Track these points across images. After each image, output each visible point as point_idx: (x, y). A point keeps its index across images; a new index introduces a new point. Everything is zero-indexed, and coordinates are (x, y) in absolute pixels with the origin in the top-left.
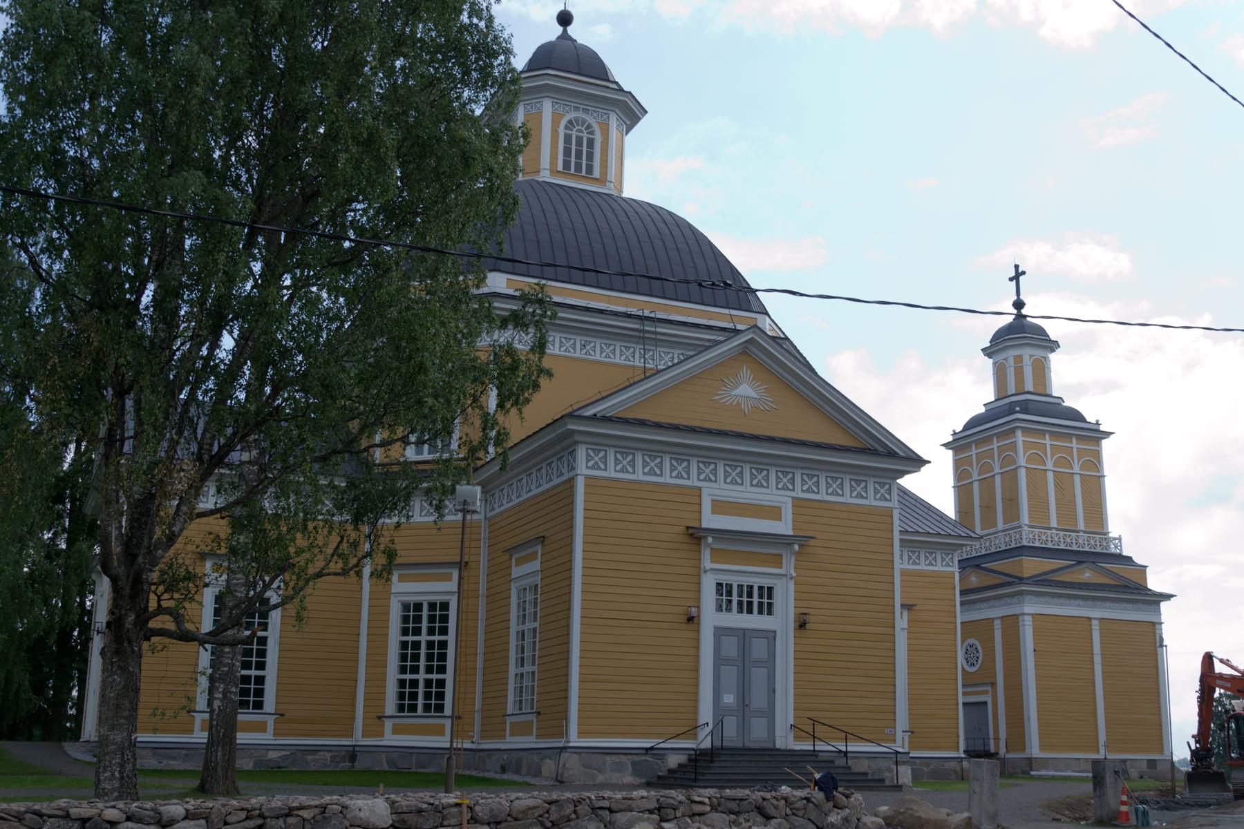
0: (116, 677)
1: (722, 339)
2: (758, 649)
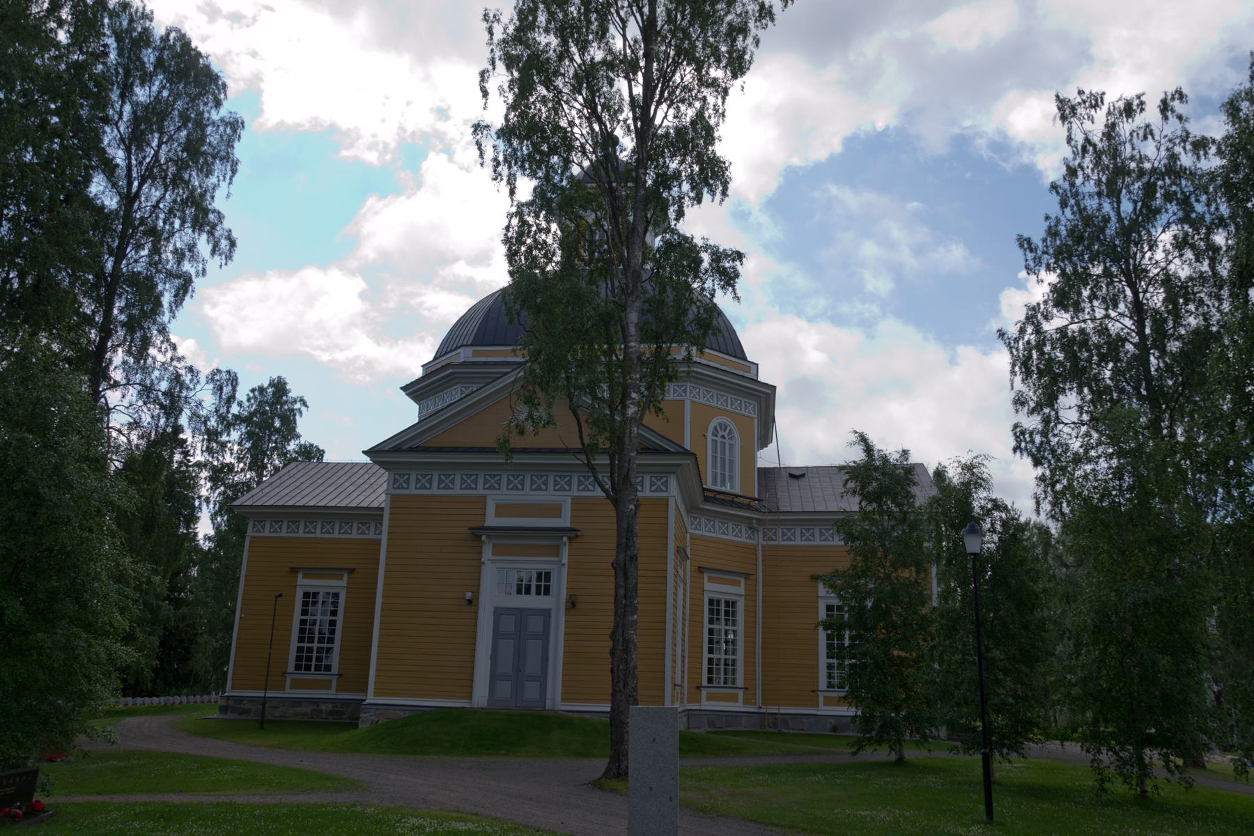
1: (508, 370)
2: (535, 624)
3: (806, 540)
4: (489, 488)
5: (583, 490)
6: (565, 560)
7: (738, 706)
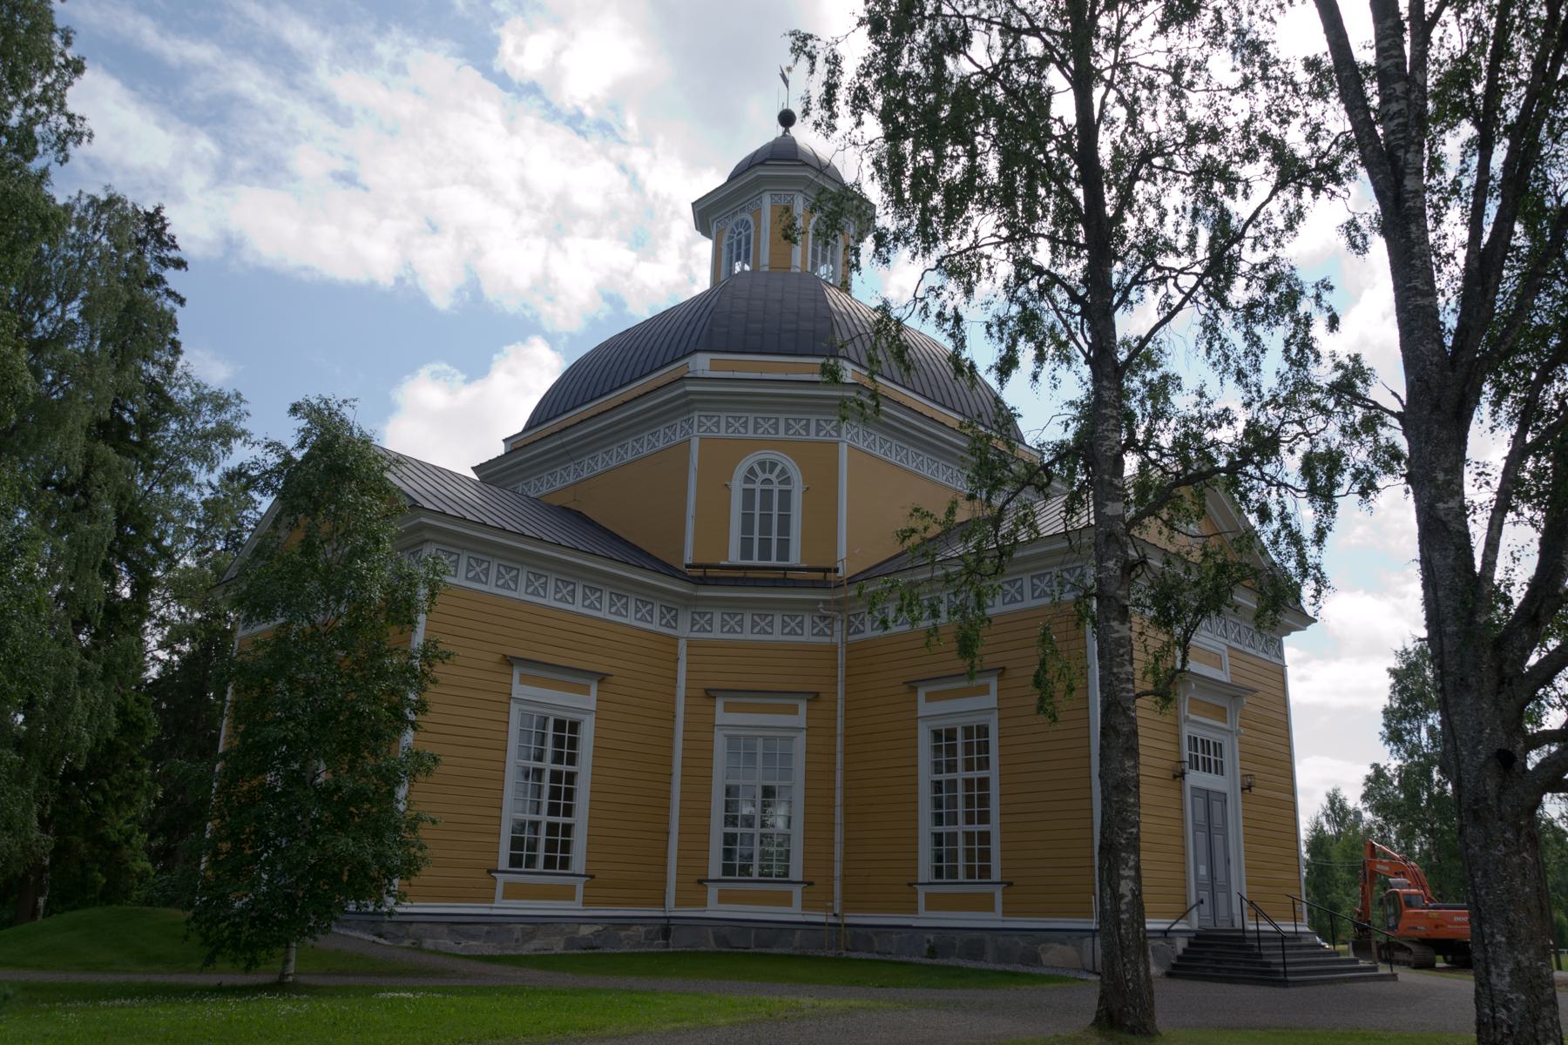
0: (1525, 855)
3: (759, 633)
7: (793, 912)
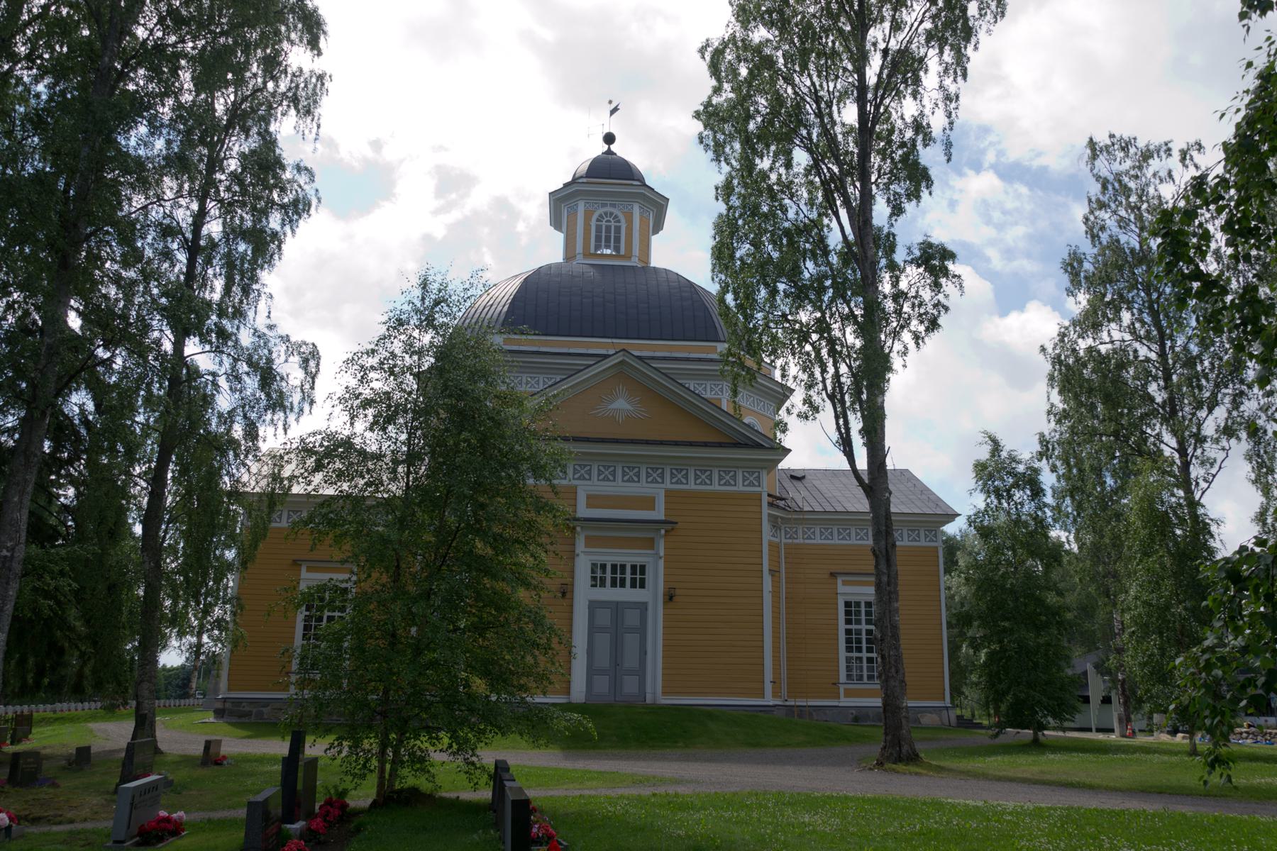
2: (632, 618)
4: (579, 479)
5: (676, 483)
6: (662, 554)
